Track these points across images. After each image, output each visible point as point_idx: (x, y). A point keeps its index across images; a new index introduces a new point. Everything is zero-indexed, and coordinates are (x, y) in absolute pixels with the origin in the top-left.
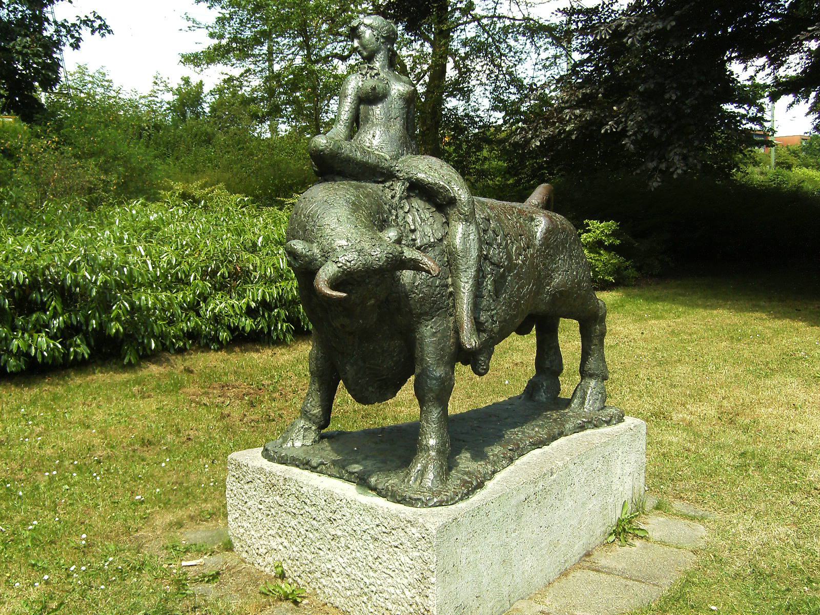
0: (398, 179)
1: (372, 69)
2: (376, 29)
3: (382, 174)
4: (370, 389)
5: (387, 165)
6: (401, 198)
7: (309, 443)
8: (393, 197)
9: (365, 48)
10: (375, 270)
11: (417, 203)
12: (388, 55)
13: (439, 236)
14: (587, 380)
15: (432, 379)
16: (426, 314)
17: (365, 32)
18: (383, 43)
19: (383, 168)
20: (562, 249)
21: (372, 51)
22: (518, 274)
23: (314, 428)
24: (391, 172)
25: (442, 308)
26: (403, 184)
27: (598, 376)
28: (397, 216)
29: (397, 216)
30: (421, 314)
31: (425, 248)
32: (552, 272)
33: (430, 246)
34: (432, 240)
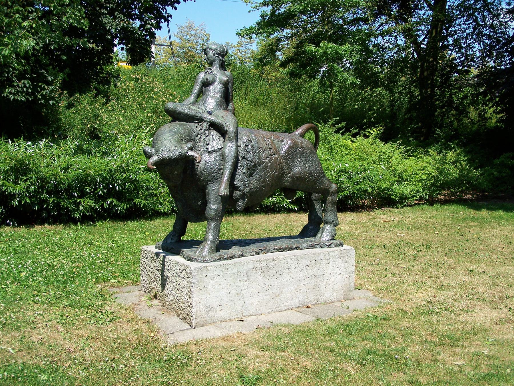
0: (205, 122)
1: (210, 69)
2: (214, 51)
3: (197, 119)
4: (191, 215)
5: (200, 115)
6: (205, 130)
7: (173, 241)
8: (201, 130)
9: (208, 60)
10: (173, 159)
11: (214, 133)
12: (220, 62)
13: (219, 147)
14: (326, 225)
15: (211, 209)
16: (210, 181)
17: (210, 52)
18: (217, 57)
19: (197, 116)
20: (300, 156)
21: (212, 61)
22: (265, 166)
23: (177, 235)
24: (202, 118)
25: (218, 179)
26: (207, 124)
27: (331, 223)
28: (201, 138)
29: (201, 138)
30: (208, 181)
31: (212, 152)
32: (292, 167)
33: (214, 151)
34: (216, 149)
